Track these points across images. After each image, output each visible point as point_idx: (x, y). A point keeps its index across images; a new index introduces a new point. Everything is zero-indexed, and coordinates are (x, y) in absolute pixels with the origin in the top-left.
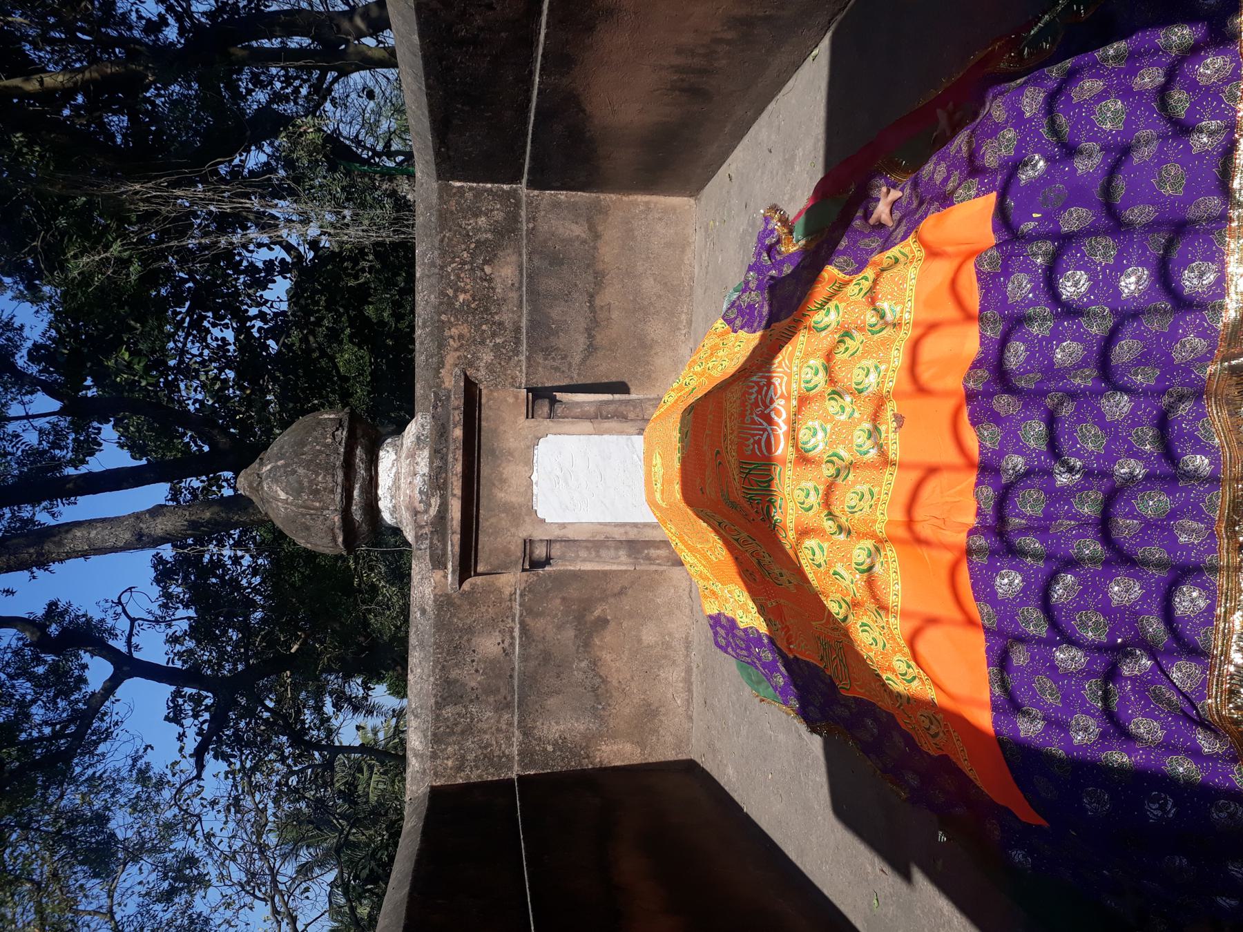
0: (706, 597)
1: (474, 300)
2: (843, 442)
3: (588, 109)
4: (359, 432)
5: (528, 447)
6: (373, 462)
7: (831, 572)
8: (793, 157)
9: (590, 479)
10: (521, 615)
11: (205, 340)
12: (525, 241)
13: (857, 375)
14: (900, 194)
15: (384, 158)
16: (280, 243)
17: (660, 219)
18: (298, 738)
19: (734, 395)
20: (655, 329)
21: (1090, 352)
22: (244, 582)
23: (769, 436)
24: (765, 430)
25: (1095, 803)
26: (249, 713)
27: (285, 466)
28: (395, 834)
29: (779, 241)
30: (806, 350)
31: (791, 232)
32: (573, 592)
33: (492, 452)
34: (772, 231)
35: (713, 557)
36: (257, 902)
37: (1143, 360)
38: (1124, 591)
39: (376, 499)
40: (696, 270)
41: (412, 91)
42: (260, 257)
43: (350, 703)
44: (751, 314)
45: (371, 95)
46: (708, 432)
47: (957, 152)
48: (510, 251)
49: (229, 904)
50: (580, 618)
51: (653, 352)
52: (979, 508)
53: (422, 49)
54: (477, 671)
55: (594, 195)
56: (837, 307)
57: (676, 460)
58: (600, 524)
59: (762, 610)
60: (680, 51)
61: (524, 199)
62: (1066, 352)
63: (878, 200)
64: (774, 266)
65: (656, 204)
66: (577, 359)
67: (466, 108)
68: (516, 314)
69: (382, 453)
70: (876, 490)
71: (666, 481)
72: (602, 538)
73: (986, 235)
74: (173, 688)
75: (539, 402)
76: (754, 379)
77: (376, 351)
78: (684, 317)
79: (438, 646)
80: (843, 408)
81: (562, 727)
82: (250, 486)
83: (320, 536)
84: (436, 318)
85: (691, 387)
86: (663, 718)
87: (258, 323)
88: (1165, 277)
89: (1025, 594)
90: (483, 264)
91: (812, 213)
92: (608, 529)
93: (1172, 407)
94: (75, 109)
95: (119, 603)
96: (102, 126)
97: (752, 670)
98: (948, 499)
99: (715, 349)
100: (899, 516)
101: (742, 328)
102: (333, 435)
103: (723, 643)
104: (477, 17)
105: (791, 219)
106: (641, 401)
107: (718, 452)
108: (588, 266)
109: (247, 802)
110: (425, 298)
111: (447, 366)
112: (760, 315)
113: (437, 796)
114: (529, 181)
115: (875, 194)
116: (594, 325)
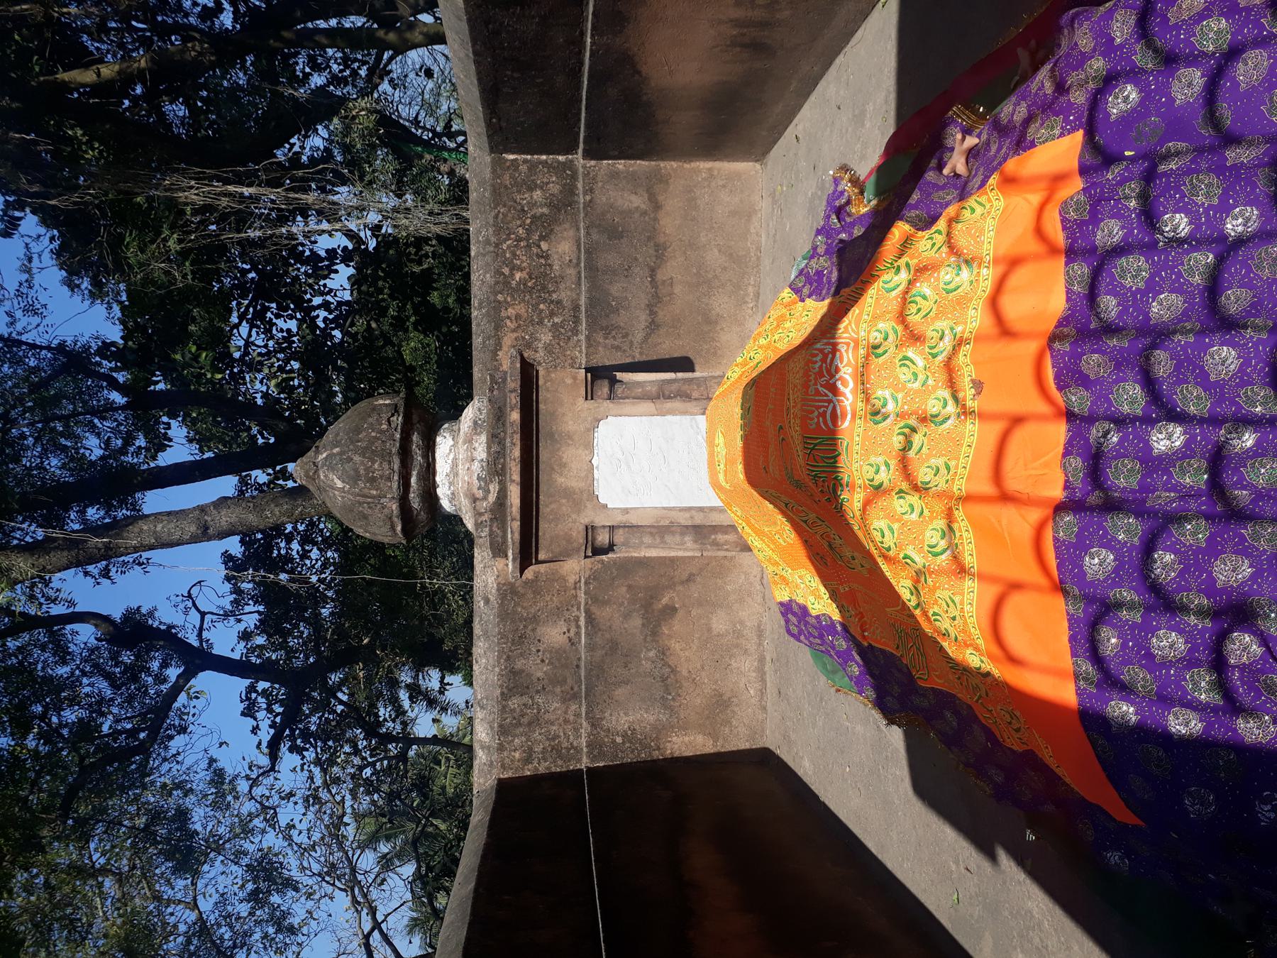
0: (776, 583)
1: (531, 278)
3: (644, 70)
4: (415, 418)
5: (588, 430)
6: (430, 448)
8: (863, 113)
9: (652, 462)
10: (586, 604)
11: (270, 331)
12: (582, 215)
14: (976, 141)
15: (445, 139)
17: (724, 186)
18: (372, 729)
19: (797, 366)
20: (721, 303)
21: (1192, 305)
23: (834, 407)
25: (1198, 804)
26: (323, 706)
27: (341, 453)
28: (464, 826)
29: (849, 202)
31: (862, 193)
32: (639, 579)
33: (551, 435)
34: (842, 193)
36: (337, 893)
41: (460, 59)
42: (324, 244)
44: (820, 281)
45: (429, 73)
46: (770, 406)
47: (1039, 89)
48: (567, 226)
49: (311, 894)
50: (647, 606)
52: (1066, 481)
53: (467, 12)
54: (543, 661)
56: (907, 265)
57: (739, 438)
58: (664, 508)
59: (834, 596)
61: (581, 170)
63: (952, 149)
64: (843, 229)
65: (719, 170)
66: (639, 336)
67: (516, 75)
69: (439, 439)
70: (952, 463)
71: (730, 462)
72: (667, 523)
74: (247, 682)
76: (818, 346)
78: (750, 289)
79: (502, 635)
80: (915, 375)
81: (631, 718)
82: (307, 476)
83: (381, 526)
84: (492, 298)
85: (755, 361)
86: (736, 709)
87: (323, 314)
89: (1118, 575)
90: (540, 240)
91: (882, 171)
92: (673, 513)
94: (135, 100)
95: (190, 596)
96: (162, 116)
97: (826, 659)
98: (1033, 472)
99: (781, 319)
102: (389, 421)
103: (795, 630)
105: (862, 178)
106: (705, 379)
107: (781, 428)
108: (649, 238)
111: (505, 348)
112: (829, 282)
113: (503, 787)
115: (949, 142)
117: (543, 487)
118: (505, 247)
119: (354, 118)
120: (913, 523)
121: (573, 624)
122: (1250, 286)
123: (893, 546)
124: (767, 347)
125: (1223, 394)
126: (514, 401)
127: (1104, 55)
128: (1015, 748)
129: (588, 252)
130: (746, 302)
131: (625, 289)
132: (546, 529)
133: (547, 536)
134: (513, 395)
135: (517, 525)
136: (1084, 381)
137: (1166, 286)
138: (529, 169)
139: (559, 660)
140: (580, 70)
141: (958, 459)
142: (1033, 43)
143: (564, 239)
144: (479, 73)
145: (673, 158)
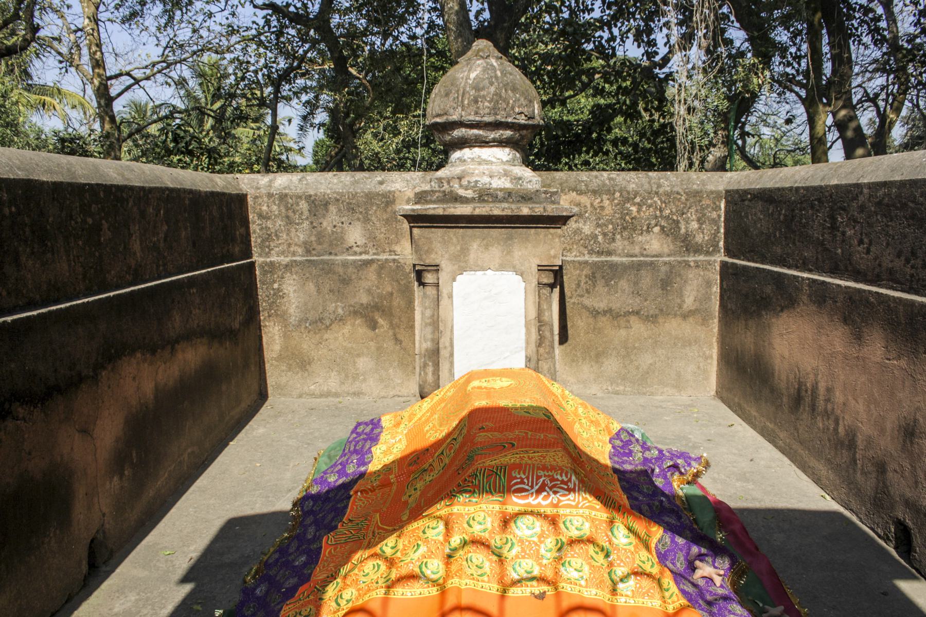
0: (395, 417)
1: (632, 219)
2: (523, 550)
3: (784, 315)
5: (514, 267)
6: (501, 143)
7: (419, 542)
8: (747, 480)
9: (488, 320)
10: (378, 260)
12: (679, 259)
13: (577, 562)
16: (670, 52)
17: (699, 367)
22: (402, 29)
23: (526, 490)
24: (532, 487)
27: (496, 77)
29: (681, 473)
30: (596, 520)
31: (688, 483)
33: (510, 238)
35: (427, 428)
39: (471, 147)
41: (793, 175)
42: (660, 37)
43: (309, 114)
44: (625, 454)
45: (788, 121)
48: (672, 247)
50: (377, 307)
51: (593, 363)
53: (827, 186)
54: (335, 226)
55: (717, 314)
56: (630, 544)
58: (452, 327)
59: (387, 469)
60: (829, 390)
61: (713, 259)
64: (662, 470)
65: (711, 364)
66: (587, 301)
67: (782, 217)
68: (622, 252)
69: (507, 150)
70: (486, 578)
71: (489, 392)
72: (441, 328)
75: (552, 275)
76: (574, 478)
77: (588, 128)
78: (622, 388)
79: (354, 196)
81: (292, 295)
82: (479, 51)
83: (440, 104)
87: (606, 35)
92: (449, 333)
99: (596, 423)
100: (465, 601)
101: (613, 447)
102: (522, 113)
103: (360, 430)
104: (853, 232)
106: (553, 358)
107: (513, 445)
108: (661, 310)
112: (623, 463)
116: (613, 315)
117: (470, 232)
118: (656, 199)
123: (426, 536)
124: (576, 414)
126: (537, 210)
129: (652, 263)
130: (612, 384)
131: (623, 291)
132: (437, 234)
133: (431, 235)
134: (542, 210)
135: (440, 212)
138: (713, 219)
139: (336, 239)
140: (785, 266)
141: (489, 582)
143: (662, 245)
144: (783, 189)
145: (720, 330)
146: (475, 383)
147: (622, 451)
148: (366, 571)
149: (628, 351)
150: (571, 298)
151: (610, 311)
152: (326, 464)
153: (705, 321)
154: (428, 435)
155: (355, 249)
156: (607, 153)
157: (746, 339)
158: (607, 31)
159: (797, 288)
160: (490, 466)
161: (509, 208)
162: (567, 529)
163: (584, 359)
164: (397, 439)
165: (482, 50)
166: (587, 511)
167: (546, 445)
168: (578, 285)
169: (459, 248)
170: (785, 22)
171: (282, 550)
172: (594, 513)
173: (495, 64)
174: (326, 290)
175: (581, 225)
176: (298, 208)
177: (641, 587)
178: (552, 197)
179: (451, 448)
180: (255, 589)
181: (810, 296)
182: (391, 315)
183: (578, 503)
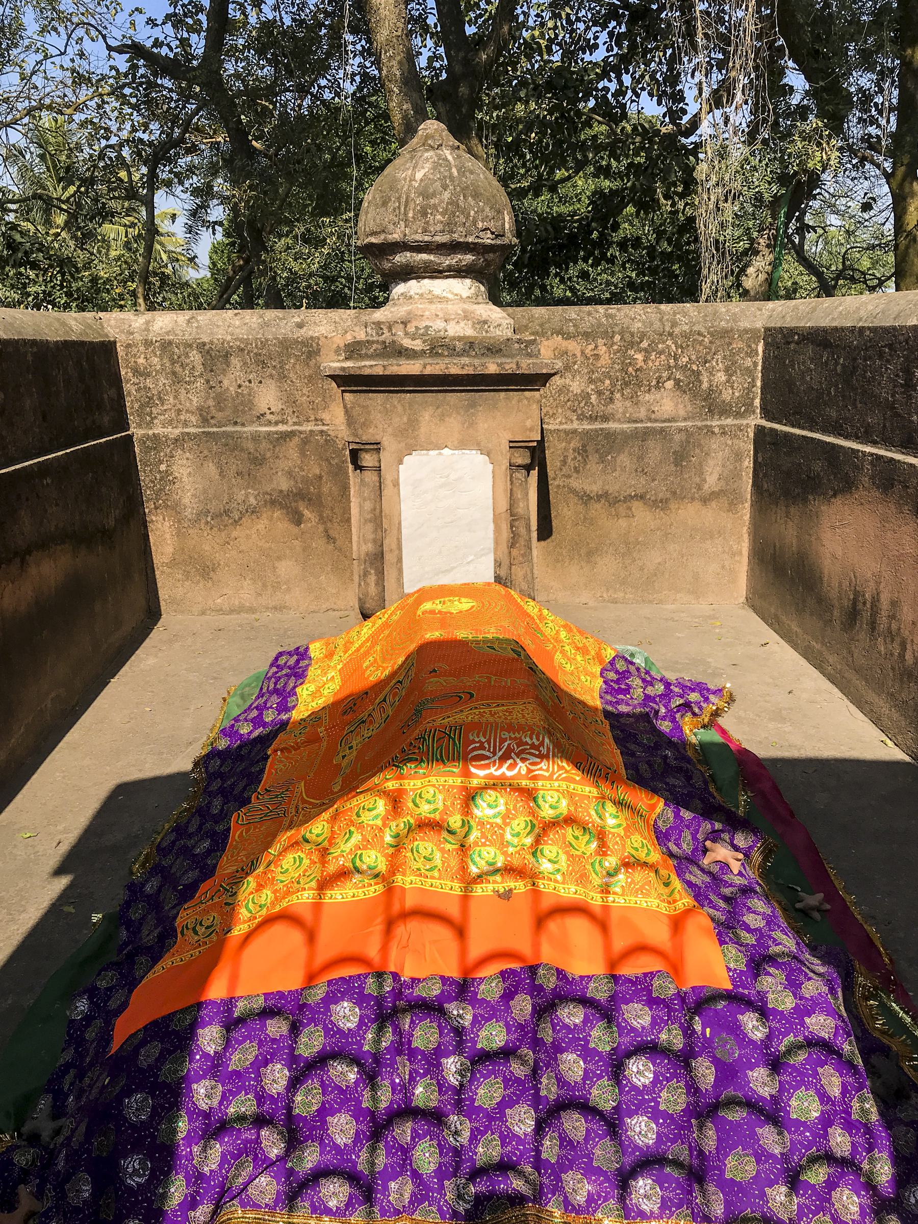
0: (327, 644)
2: (483, 835)
3: (838, 501)
5: (478, 444)
6: (459, 272)
7: (352, 829)
8: (783, 720)
9: (446, 503)
10: (301, 432)
12: (699, 424)
17: (723, 567)
18: (159, 155)
23: (488, 758)
24: (494, 753)
27: (451, 177)
29: (694, 714)
31: (704, 727)
33: (473, 405)
37: (565, 1142)
38: (342, 1128)
40: (669, 607)
44: (620, 691)
45: (866, 207)
47: (775, 940)
48: (689, 408)
50: (301, 495)
52: (419, 980)
53: (902, 327)
54: (240, 386)
56: (619, 825)
58: (400, 523)
59: (316, 717)
60: (894, 604)
61: (745, 422)
62: (573, 1065)
65: (740, 562)
66: (575, 483)
67: (839, 368)
68: (622, 416)
69: (468, 282)
71: (444, 619)
72: (385, 526)
73: (693, 979)
75: (528, 453)
76: (547, 740)
78: (620, 595)
79: (264, 343)
81: (185, 479)
82: (428, 137)
84: (617, 329)
86: (201, 585)
87: (613, 86)
88: (649, 1162)
89: (335, 1033)
90: (675, 379)
92: (395, 532)
93: (521, 1174)
99: (584, 651)
100: (410, 902)
106: (531, 561)
107: (472, 696)
108: (674, 493)
109: (85, 93)
110: (638, 315)
112: (618, 703)
113: (105, 351)
114: (763, 428)
118: (669, 342)
119: (819, 144)
120: (382, 837)
121: (279, 418)
122: (587, 1139)
124: (557, 640)
125: (495, 1119)
126: (507, 367)
127: (796, 1008)
128: (178, 920)
129: (662, 430)
130: (608, 590)
132: (376, 401)
134: (515, 367)
135: (379, 371)
136: (508, 996)
137: (591, 1066)
138: (747, 368)
139: (242, 403)
140: (840, 435)
141: (439, 879)
142: (828, 907)
144: (842, 329)
146: (427, 606)
147: (616, 687)
148: (285, 867)
149: (629, 547)
150: (554, 479)
151: (606, 495)
152: (238, 706)
153: (732, 506)
154: (368, 672)
155: (269, 417)
156: (612, 261)
157: (787, 531)
158: (615, 81)
159: (857, 467)
160: (441, 726)
161: (471, 365)
162: (539, 806)
163: (572, 559)
164: (330, 676)
165: (431, 137)
166: (564, 785)
167: (512, 695)
168: (564, 462)
169: (405, 419)
170: (867, 61)
171: (180, 830)
172: (572, 786)
173: (450, 158)
174: (232, 473)
175: (567, 381)
176: (188, 361)
177: (633, 882)
178: (528, 348)
179: (395, 695)
180: (143, 885)
181: (872, 478)
182: (320, 505)
183: (553, 773)
